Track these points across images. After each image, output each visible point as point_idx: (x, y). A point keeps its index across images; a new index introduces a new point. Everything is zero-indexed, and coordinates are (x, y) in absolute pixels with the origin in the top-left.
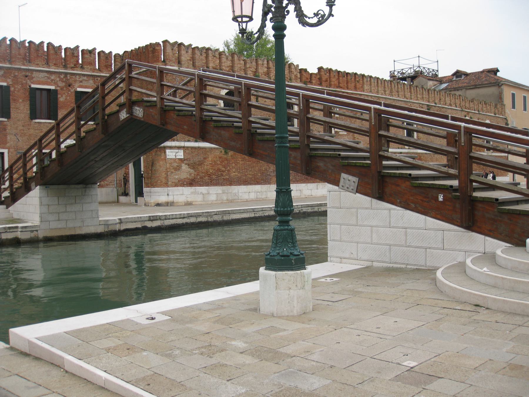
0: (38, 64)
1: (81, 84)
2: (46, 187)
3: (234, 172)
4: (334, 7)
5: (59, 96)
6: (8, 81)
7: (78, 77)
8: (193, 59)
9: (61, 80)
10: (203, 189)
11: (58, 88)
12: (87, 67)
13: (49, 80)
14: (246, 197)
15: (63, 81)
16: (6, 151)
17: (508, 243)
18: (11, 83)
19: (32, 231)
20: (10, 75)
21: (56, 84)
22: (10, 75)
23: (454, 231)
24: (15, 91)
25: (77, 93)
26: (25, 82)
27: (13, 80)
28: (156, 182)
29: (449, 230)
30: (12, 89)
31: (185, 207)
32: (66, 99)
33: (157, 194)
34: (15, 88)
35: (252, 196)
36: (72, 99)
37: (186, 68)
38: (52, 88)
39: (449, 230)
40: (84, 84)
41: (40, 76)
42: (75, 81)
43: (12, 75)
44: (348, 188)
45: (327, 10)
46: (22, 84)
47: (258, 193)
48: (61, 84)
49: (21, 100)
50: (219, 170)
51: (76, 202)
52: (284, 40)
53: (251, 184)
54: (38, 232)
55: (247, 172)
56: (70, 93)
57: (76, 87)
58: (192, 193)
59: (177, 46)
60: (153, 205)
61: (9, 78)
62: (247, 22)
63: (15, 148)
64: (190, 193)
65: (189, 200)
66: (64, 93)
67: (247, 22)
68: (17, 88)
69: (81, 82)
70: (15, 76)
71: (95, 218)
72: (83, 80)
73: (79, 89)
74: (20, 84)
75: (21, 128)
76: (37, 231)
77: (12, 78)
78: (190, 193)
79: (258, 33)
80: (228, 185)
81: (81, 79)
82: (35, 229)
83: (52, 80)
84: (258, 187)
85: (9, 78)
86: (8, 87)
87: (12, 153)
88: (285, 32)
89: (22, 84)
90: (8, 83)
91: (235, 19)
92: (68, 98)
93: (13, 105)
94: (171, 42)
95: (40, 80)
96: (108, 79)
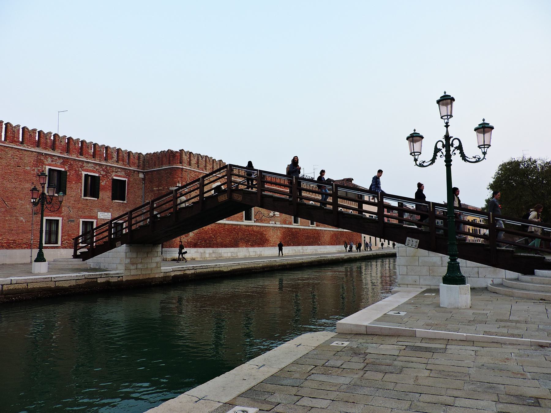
0: (87, 157)
1: (116, 174)
2: (130, 245)
3: (219, 239)
4: (486, 155)
5: (101, 181)
6: (66, 167)
7: (114, 169)
8: (198, 163)
9: (103, 170)
10: (201, 250)
11: (101, 176)
12: (121, 162)
13: (95, 170)
14: (225, 255)
15: (104, 171)
16: (60, 219)
17: (519, 273)
18: (67, 169)
19: (119, 277)
20: (68, 163)
21: (99, 172)
22: (68, 163)
23: (485, 267)
24: (70, 175)
25: (114, 180)
26: (78, 169)
27: (69, 167)
28: (173, 244)
29: (482, 267)
30: (68, 173)
31: (171, 261)
32: (106, 184)
33: (174, 252)
34: (70, 173)
35: (229, 255)
36: (110, 184)
37: (194, 169)
38: (97, 175)
39: (482, 267)
40: (118, 174)
41: (89, 166)
42: (113, 171)
43: (69, 163)
44: (412, 245)
45: (482, 156)
46: (76, 171)
47: (232, 253)
48: (102, 173)
49: (74, 182)
50: (211, 237)
51: (148, 256)
52: (451, 167)
53: (229, 247)
54: (123, 277)
55: (226, 239)
56: (108, 179)
57: (113, 175)
58: (195, 252)
59: (189, 153)
60: (170, 260)
61: (67, 165)
62: (418, 155)
63: (68, 217)
64: (194, 252)
65: (194, 257)
66: (105, 180)
67: (418, 155)
68: (72, 173)
69: (116, 172)
70: (71, 164)
71: (158, 267)
72: (118, 171)
73: (115, 178)
74: (74, 171)
75: (73, 202)
76: (122, 276)
77: (69, 165)
78: (194, 252)
79: (431, 161)
80: (215, 247)
81: (116, 171)
82: (121, 275)
83: (97, 170)
84: (232, 249)
85: (67, 165)
86: (66, 172)
87: (65, 220)
88: (451, 163)
89: (76, 171)
90: (65, 169)
91: (411, 154)
92: (107, 183)
93: (68, 185)
94: (185, 151)
95: (89, 169)
96: (207, 175)
